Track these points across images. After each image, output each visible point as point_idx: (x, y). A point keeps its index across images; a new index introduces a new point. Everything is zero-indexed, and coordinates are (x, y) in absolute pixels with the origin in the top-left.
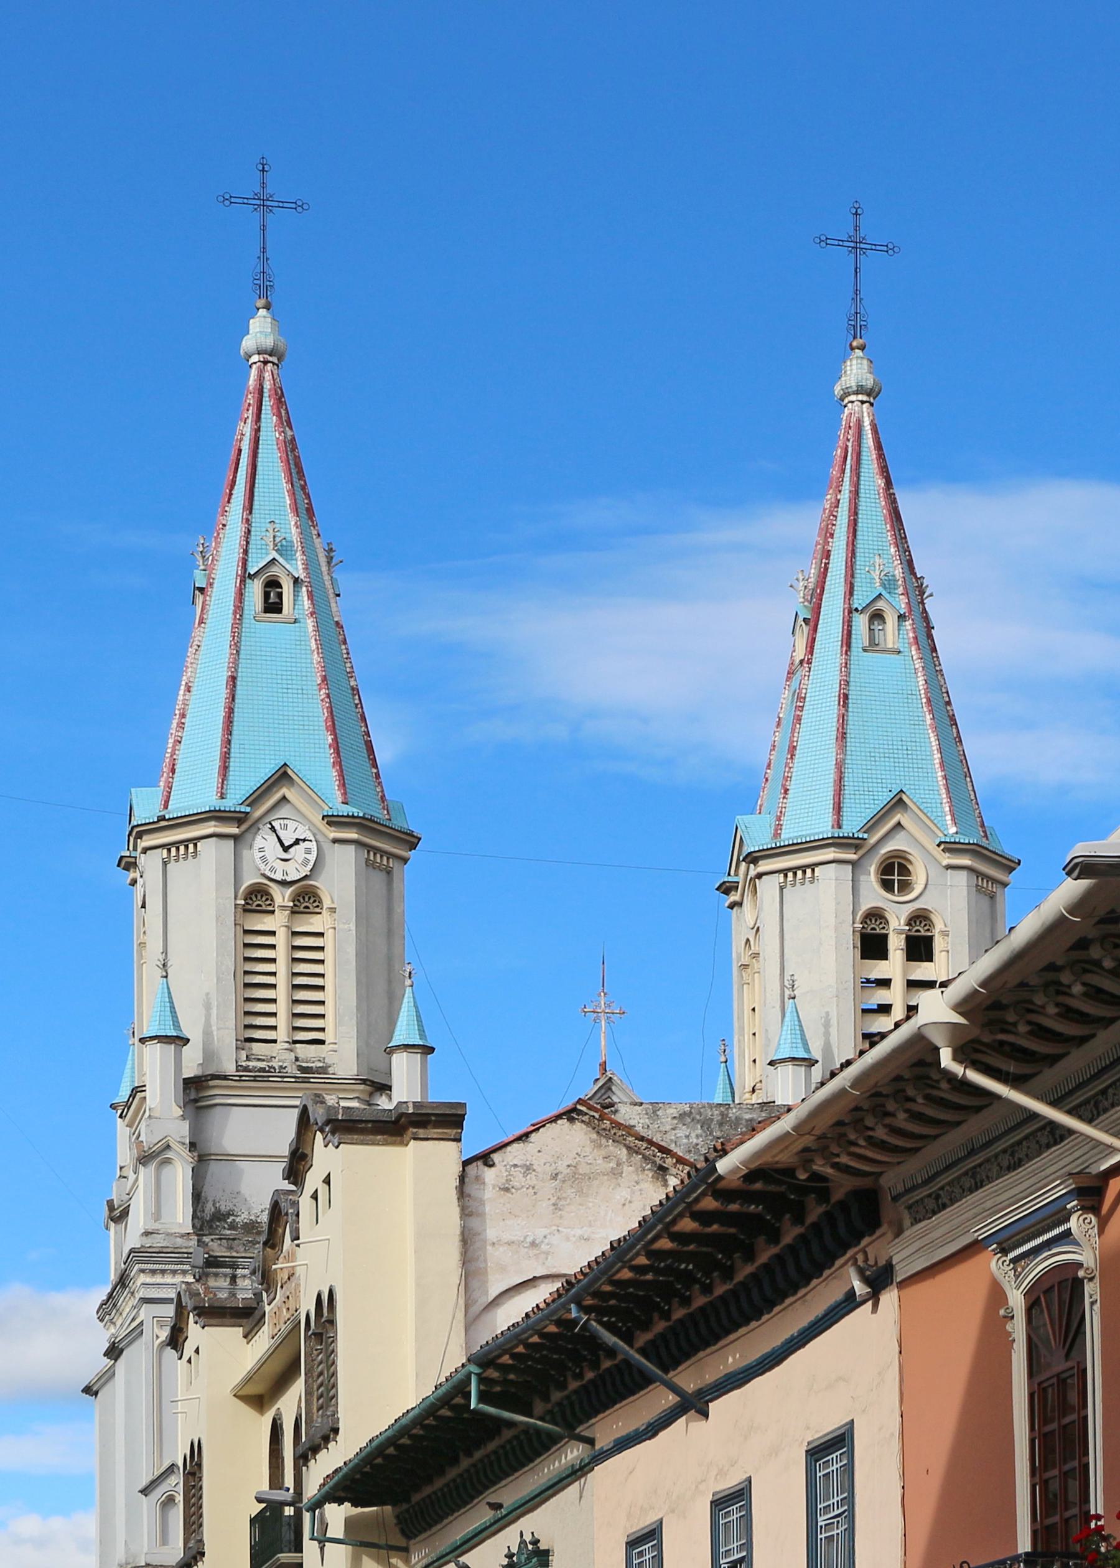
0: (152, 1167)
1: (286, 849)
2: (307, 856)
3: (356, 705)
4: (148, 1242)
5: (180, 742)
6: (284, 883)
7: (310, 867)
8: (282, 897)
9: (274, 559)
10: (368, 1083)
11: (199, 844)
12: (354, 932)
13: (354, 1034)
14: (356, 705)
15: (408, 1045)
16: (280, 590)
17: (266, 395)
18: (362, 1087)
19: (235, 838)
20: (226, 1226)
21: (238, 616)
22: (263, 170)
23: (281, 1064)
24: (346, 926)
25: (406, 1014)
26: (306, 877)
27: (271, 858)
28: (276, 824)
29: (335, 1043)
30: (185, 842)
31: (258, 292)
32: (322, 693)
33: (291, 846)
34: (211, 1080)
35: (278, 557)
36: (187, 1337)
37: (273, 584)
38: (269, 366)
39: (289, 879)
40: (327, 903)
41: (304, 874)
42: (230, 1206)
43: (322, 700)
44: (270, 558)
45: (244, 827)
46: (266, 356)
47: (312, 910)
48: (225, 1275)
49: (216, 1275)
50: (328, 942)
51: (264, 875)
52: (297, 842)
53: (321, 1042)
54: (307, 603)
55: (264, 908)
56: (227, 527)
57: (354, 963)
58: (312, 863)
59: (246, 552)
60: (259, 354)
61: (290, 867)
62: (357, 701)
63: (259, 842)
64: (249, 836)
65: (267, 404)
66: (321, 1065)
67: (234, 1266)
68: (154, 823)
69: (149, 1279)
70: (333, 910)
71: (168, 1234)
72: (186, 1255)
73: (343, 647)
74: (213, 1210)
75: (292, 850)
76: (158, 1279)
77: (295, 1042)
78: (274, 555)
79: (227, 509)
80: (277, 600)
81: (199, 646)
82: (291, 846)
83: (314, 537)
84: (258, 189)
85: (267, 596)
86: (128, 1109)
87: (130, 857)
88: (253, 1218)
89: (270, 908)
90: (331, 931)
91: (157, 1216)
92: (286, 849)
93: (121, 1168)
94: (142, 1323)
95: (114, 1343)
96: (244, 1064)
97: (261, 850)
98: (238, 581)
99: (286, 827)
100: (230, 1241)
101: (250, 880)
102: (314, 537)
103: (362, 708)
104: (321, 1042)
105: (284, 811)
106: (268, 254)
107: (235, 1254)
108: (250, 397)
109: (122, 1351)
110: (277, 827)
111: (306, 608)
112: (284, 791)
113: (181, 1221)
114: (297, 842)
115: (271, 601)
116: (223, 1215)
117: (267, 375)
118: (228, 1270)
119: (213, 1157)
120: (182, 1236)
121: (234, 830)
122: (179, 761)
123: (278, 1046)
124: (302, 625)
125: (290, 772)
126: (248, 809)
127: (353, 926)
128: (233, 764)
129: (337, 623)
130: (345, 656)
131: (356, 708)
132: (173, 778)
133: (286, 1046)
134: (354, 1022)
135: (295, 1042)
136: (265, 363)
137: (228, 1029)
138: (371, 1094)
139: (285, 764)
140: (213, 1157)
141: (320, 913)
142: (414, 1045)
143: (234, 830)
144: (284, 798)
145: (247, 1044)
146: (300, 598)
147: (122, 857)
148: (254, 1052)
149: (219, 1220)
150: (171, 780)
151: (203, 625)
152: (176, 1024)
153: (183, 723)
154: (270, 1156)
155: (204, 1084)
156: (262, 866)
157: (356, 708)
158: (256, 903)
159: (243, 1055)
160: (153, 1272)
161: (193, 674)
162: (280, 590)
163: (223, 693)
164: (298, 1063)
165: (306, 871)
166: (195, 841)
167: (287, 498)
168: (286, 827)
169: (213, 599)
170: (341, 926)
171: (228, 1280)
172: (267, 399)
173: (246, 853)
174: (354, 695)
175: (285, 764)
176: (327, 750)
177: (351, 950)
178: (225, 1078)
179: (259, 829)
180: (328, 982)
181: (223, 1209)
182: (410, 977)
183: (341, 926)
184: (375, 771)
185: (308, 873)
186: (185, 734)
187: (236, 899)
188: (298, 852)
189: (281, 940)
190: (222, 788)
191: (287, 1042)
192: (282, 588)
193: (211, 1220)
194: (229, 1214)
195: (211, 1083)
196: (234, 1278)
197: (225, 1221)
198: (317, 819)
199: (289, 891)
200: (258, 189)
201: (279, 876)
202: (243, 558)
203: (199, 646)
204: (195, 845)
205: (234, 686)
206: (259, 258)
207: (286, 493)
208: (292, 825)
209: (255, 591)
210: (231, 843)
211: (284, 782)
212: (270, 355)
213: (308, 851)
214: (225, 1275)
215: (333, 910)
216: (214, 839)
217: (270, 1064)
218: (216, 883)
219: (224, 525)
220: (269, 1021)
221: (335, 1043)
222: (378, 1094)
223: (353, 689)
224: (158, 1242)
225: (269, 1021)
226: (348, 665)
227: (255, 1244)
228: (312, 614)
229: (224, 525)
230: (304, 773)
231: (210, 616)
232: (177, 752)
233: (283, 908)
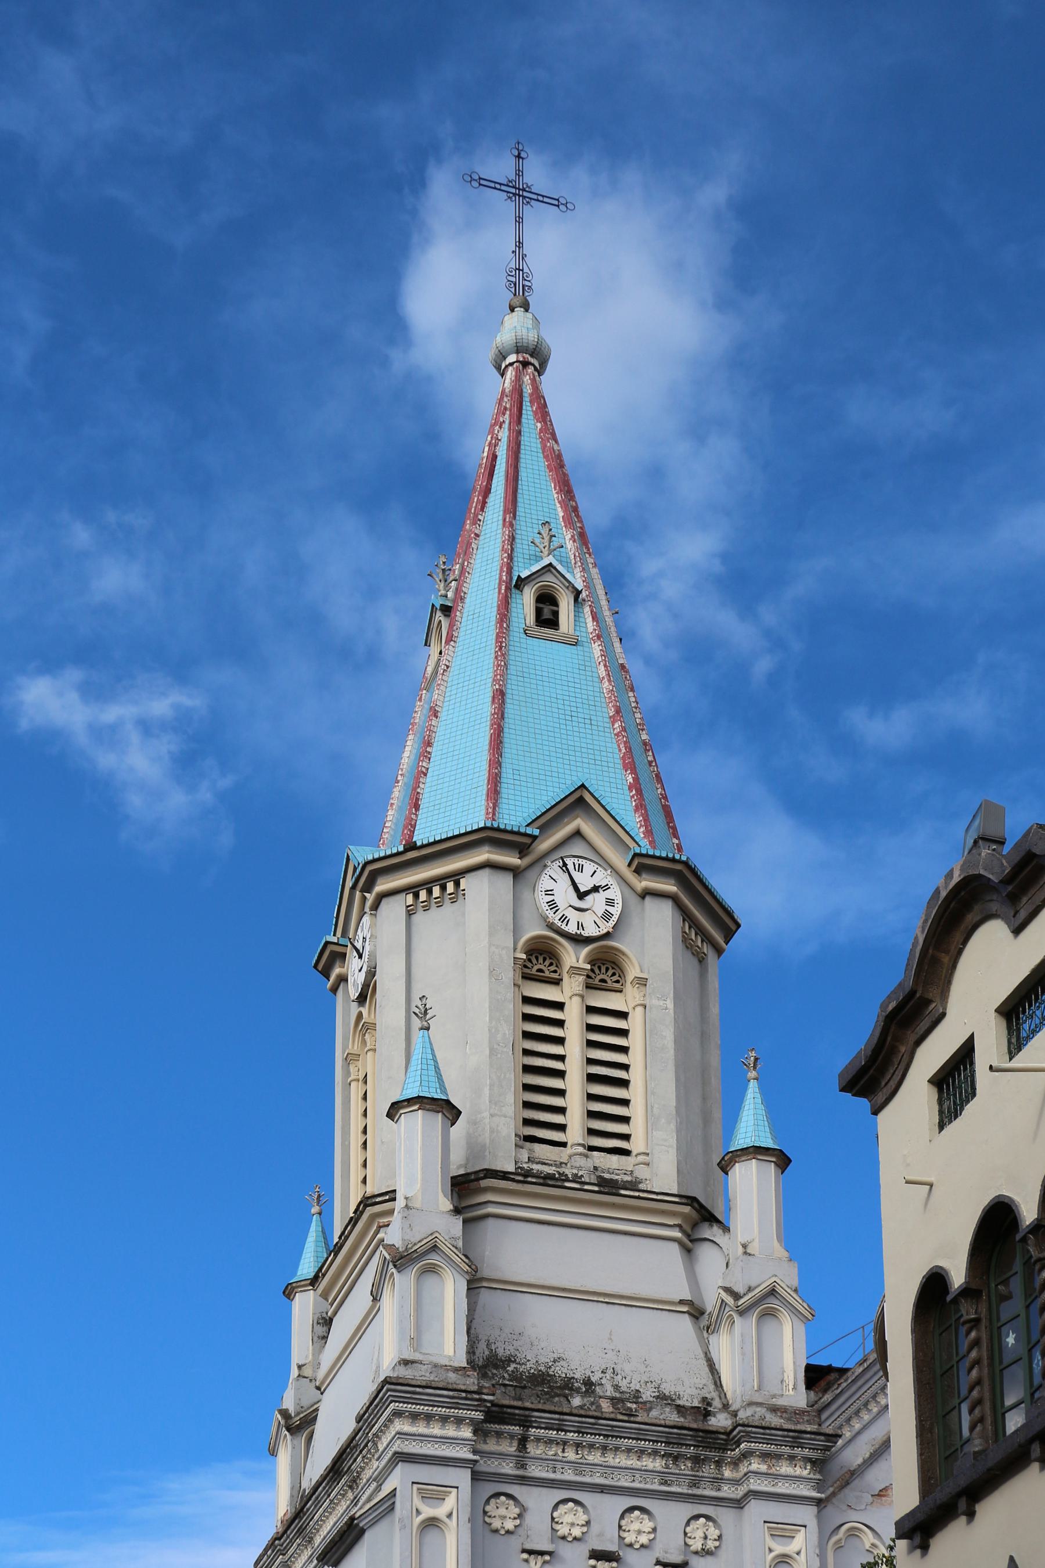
0: (411, 1274)
1: (581, 896)
2: (609, 909)
3: (650, 763)
4: (404, 1372)
5: (425, 775)
6: (578, 940)
7: (612, 923)
8: (573, 957)
9: (550, 564)
10: (696, 1205)
11: (462, 881)
12: (672, 1012)
13: (673, 1141)
14: (650, 763)
15: (760, 1147)
16: (555, 608)
17: (526, 399)
18: (687, 1209)
19: (516, 872)
20: (506, 1375)
21: (505, 625)
22: (519, 157)
23: (575, 1171)
24: (661, 1003)
25: (752, 1112)
26: (607, 935)
27: (562, 904)
28: (569, 862)
29: (648, 1154)
30: (441, 881)
31: (513, 290)
32: (616, 725)
33: (587, 893)
34: (485, 1177)
35: (555, 563)
36: (943, 1015)
37: (546, 600)
38: (530, 369)
39: (586, 933)
40: (632, 972)
41: (605, 931)
42: (510, 1350)
43: (617, 735)
44: (545, 562)
45: (527, 860)
46: (527, 356)
47: (610, 984)
48: (512, 1437)
49: (499, 1434)
50: (635, 1024)
51: (551, 926)
52: (596, 889)
53: (626, 1153)
54: (590, 625)
55: (547, 974)
56: (481, 538)
57: (672, 1052)
58: (615, 918)
59: (511, 557)
60: (517, 352)
61: (587, 919)
62: (650, 758)
63: (545, 883)
64: (531, 874)
65: (528, 410)
66: (628, 1178)
67: (526, 1423)
68: (398, 854)
69: (407, 1428)
70: (642, 982)
71: (436, 1366)
72: (464, 1395)
73: (631, 694)
74: (487, 1353)
75: (589, 898)
76: (421, 1428)
77: (592, 1148)
78: (550, 559)
79: (480, 517)
80: (551, 617)
81: (448, 667)
82: (587, 893)
83: (591, 566)
84: (512, 177)
85: (539, 612)
86: (336, 1256)
87: (337, 944)
88: (542, 1368)
89: (555, 976)
90: (640, 1009)
91: (416, 1342)
92: (581, 896)
93: (300, 1367)
94: (393, 1493)
95: (352, 1519)
96: (525, 1166)
97: (549, 892)
98: (503, 587)
99: (581, 868)
100: (518, 1389)
101: (534, 930)
102: (591, 566)
103: (656, 765)
104: (626, 1153)
105: (578, 848)
106: (526, 250)
107: (528, 1405)
108: (505, 399)
109: (362, 1532)
110: (570, 867)
111: (590, 629)
112: (579, 822)
113: (451, 1353)
114: (596, 889)
115: (545, 617)
116: (501, 1360)
117: (527, 379)
118: (516, 1429)
119: (485, 1284)
120: (456, 1370)
121: (513, 860)
122: (425, 796)
123: (568, 1151)
124: (586, 649)
125: (588, 798)
126: (536, 832)
127: (670, 1004)
128: (505, 790)
129: (622, 666)
130: (633, 705)
131: (651, 766)
132: (417, 815)
133: (581, 1149)
134: (673, 1126)
135: (592, 1148)
136: (525, 364)
137: (505, 1117)
138: (695, 1226)
139: (583, 786)
140: (485, 1284)
141: (621, 991)
142: (768, 1149)
143: (513, 860)
144: (578, 834)
145: (528, 1144)
146: (581, 620)
147: (327, 943)
148: (536, 1155)
149: (496, 1367)
150: (413, 816)
151: (452, 643)
152: (443, 1089)
153: (429, 753)
154: (564, 1290)
155: (473, 1185)
156: (550, 914)
157: (651, 766)
158: (536, 968)
159: (524, 1155)
160: (414, 1417)
161: (441, 698)
162: (555, 608)
163: (486, 709)
164: (599, 1173)
165: (606, 927)
166: (456, 877)
167: (560, 509)
168: (581, 868)
169: (465, 615)
170: (655, 1002)
171: (515, 1443)
172: (528, 404)
173: (526, 895)
174: (647, 750)
175: (583, 786)
176: (627, 792)
177: (668, 1035)
178: (504, 1176)
179: (545, 866)
180: (636, 1076)
181: (501, 1352)
182: (755, 1067)
183: (655, 1002)
184: (676, 841)
185: (611, 930)
186: (431, 764)
187: (515, 950)
188: (596, 902)
189: (573, 1016)
190: (494, 814)
191: (583, 1145)
192: (557, 605)
193: (485, 1367)
194: (509, 1360)
195: (485, 1183)
196: (523, 1441)
197: (504, 1368)
198: (620, 862)
199: (586, 951)
200: (512, 177)
201: (572, 928)
202: (508, 564)
203: (448, 667)
204: (457, 884)
205: (503, 702)
206: (513, 252)
207: (558, 505)
208: (589, 867)
209: (526, 603)
210: (507, 879)
211: (578, 811)
212: (532, 356)
213: (610, 902)
214: (512, 1437)
215: (642, 982)
216: (485, 873)
217: (561, 1170)
218: (490, 927)
219: (477, 535)
220: (557, 1119)
221: (648, 1154)
222: (706, 1224)
223: (645, 743)
224: (419, 1374)
225: (557, 1119)
226: (638, 715)
227: (553, 1397)
228: (599, 637)
229: (477, 535)
230: (609, 800)
231: (461, 634)
232: (421, 785)
233: (575, 970)
